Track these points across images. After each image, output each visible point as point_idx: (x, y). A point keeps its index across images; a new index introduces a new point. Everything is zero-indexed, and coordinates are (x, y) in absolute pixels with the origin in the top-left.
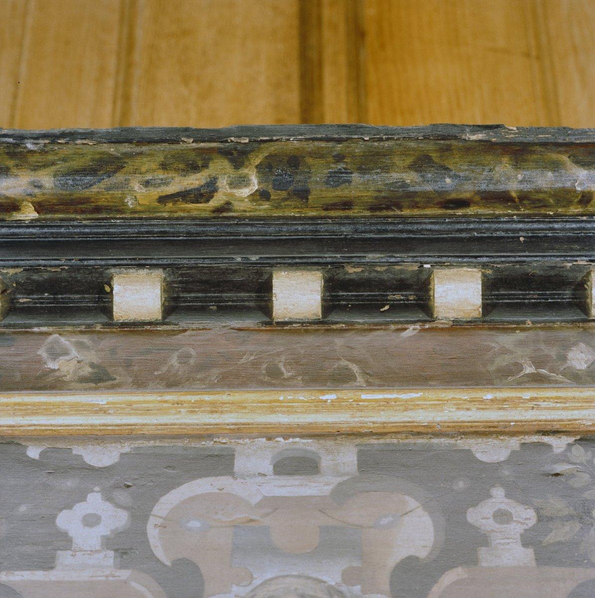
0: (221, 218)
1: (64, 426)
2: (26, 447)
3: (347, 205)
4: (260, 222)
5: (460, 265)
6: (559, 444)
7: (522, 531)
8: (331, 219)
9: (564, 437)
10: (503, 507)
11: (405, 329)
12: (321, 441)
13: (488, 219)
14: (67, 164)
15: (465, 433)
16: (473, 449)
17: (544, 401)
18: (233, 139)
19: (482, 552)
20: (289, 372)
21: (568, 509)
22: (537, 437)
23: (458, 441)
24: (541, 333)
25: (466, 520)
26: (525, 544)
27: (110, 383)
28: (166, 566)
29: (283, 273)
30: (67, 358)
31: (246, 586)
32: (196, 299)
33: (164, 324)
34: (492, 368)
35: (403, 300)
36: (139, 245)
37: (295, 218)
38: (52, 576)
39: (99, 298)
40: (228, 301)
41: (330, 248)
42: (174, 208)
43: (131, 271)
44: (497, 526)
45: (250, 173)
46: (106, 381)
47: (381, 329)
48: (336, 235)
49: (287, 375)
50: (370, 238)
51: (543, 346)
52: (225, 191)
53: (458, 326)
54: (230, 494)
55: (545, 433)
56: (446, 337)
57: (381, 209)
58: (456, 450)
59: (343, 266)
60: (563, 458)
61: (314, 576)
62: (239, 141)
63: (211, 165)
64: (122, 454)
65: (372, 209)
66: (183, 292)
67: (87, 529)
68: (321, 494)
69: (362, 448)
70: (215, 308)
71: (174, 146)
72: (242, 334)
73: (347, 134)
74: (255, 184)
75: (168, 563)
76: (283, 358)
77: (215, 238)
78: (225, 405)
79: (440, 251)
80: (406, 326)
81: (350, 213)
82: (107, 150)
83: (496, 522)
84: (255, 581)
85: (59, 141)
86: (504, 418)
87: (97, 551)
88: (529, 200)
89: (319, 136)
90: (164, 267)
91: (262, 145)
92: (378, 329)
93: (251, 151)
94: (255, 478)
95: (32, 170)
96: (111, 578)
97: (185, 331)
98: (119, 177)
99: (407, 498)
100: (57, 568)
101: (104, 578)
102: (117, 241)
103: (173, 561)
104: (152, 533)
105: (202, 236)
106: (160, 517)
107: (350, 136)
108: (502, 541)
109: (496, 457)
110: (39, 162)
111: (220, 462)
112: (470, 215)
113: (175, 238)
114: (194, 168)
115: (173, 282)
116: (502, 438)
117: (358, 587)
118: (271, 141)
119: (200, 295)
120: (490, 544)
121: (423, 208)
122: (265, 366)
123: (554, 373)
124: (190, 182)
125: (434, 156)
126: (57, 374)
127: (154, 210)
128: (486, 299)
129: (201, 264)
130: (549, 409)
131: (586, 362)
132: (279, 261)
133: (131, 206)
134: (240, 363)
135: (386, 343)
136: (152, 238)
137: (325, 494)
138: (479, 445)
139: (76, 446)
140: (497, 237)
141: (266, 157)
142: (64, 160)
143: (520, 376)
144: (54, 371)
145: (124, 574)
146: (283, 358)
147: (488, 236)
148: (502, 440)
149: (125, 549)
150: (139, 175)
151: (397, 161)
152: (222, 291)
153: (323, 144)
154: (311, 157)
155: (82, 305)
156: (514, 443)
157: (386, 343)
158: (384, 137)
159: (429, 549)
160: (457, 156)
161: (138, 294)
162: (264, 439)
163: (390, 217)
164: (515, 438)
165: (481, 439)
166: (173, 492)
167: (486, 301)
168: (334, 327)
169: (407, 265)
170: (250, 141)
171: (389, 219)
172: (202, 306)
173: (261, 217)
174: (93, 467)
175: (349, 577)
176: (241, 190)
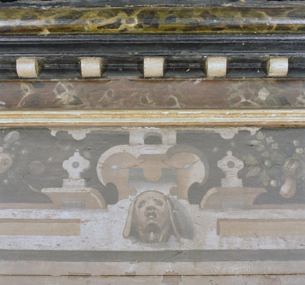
0: (123, 34)
1: (64, 123)
2: (50, 130)
3: (174, 29)
4: (139, 36)
5: (218, 56)
6: (253, 131)
7: (238, 171)
8: (167, 34)
9: (255, 128)
10: (231, 160)
11: (196, 80)
12: (163, 129)
13: (230, 35)
14: (60, 14)
15: (217, 126)
16: (221, 133)
17: (249, 114)
18: (127, 6)
19: (223, 180)
20: (150, 100)
21: (255, 161)
22: (245, 128)
23: (215, 129)
24: (249, 83)
25: (217, 166)
26: (239, 177)
27: (81, 105)
28: (104, 186)
29: (148, 59)
30: (64, 93)
31: (134, 195)
32: (114, 66)
33: (102, 78)
34: (229, 99)
35: (195, 67)
36: (90, 47)
37: (152, 34)
38: (62, 190)
39: (76, 66)
40: (126, 67)
41: (167, 48)
42: (104, 30)
43: (88, 58)
44: (229, 169)
45: (134, 17)
46: (80, 104)
47: (186, 80)
48: (169, 42)
49: (150, 102)
50: (183, 43)
51: (249, 89)
52: (124, 24)
53: (217, 80)
54: (128, 153)
55: (248, 126)
56: (211, 85)
57: (187, 30)
58: (214, 133)
59: (172, 57)
60: (255, 138)
61: (159, 191)
62: (130, 6)
63: (118, 14)
64: (87, 134)
65: (184, 30)
66: (109, 63)
67: (74, 169)
68: (162, 153)
69: (178, 132)
70: (121, 69)
71: (103, 8)
72: (132, 82)
73: (174, 4)
74: (136, 22)
75: (105, 185)
76: (148, 94)
77: (121, 43)
78: (126, 115)
79: (211, 49)
80: (196, 79)
81: (175, 32)
82: (75, 9)
83: (228, 167)
84: (138, 193)
85: (55, 7)
86: (233, 121)
87: (78, 179)
88: (247, 28)
89: (163, 5)
90: (101, 56)
91: (139, 8)
92: (185, 80)
93: (135, 10)
94: (137, 148)
95: (46, 16)
96: (83, 191)
97: (110, 81)
98: (81, 19)
99: (195, 156)
100: (63, 187)
101: (81, 191)
102: (82, 44)
103: (107, 184)
104: (99, 171)
105: (116, 42)
106: (102, 164)
107: (176, 5)
108: (230, 176)
109: (229, 137)
110: (49, 14)
111: (123, 138)
112: (223, 33)
113: (105, 43)
114: (112, 16)
115: (105, 61)
116: (232, 128)
117: (176, 196)
118: (143, 6)
119: (116, 64)
120: (226, 177)
121: (205, 30)
122: (141, 98)
123: (253, 102)
124: (110, 21)
125: (211, 12)
126: (61, 101)
127: (96, 31)
128: (228, 67)
129: (115, 55)
130: (250, 117)
131: (265, 97)
132: (146, 54)
133: (87, 30)
134: (131, 96)
135: (188, 87)
136: (96, 43)
137: (164, 153)
138: (223, 131)
139: (69, 130)
140: (234, 43)
141: (141, 12)
142: (59, 13)
143: (240, 103)
144: (59, 99)
145: (89, 189)
146: (148, 94)
147: (230, 43)
148: (231, 129)
149: (89, 178)
150: (89, 18)
151: (195, 13)
152: (124, 63)
153: (164, 7)
154: (160, 12)
155: (70, 68)
156: (236, 130)
157: (188, 87)
158: (190, 5)
159: (203, 179)
160: (220, 12)
161: (91, 66)
162: (141, 128)
163: (191, 34)
164: (237, 128)
165: (223, 129)
166: (107, 152)
167: (227, 67)
168: (168, 79)
169: (198, 55)
170: (134, 7)
171: (191, 35)
172: (117, 69)
173: (139, 33)
174: (76, 140)
175: (173, 192)
176: (131, 24)
